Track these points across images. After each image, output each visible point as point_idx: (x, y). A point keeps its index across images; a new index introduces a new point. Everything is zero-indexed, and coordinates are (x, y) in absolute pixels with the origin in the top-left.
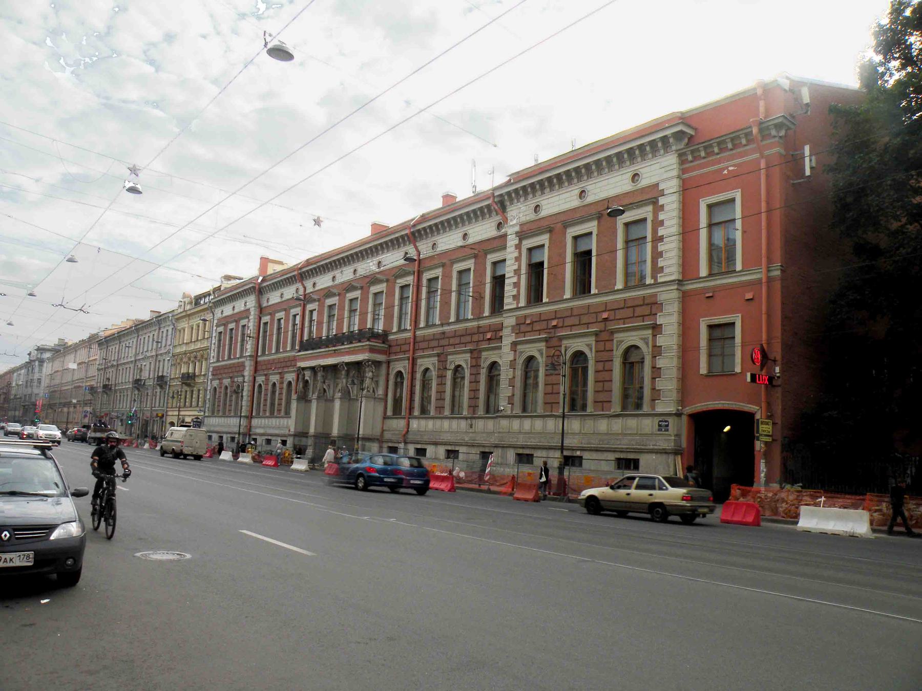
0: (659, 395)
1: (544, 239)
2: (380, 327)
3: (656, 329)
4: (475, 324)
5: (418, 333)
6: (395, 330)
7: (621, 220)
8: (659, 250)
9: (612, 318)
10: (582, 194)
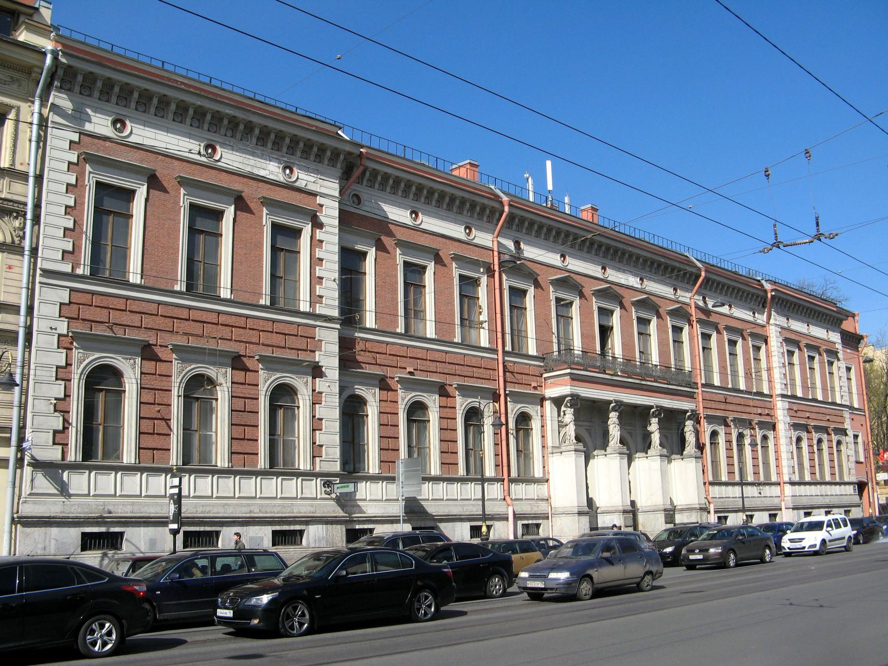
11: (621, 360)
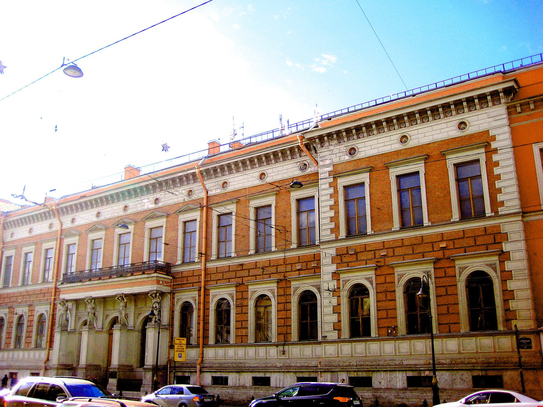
0: (515, 316)
1: (162, 222)
2: (161, 260)
3: (504, 256)
4: (281, 255)
5: (210, 265)
6: (179, 262)
7: (394, 172)
8: (497, 187)
9: (304, 268)
10: (98, 215)
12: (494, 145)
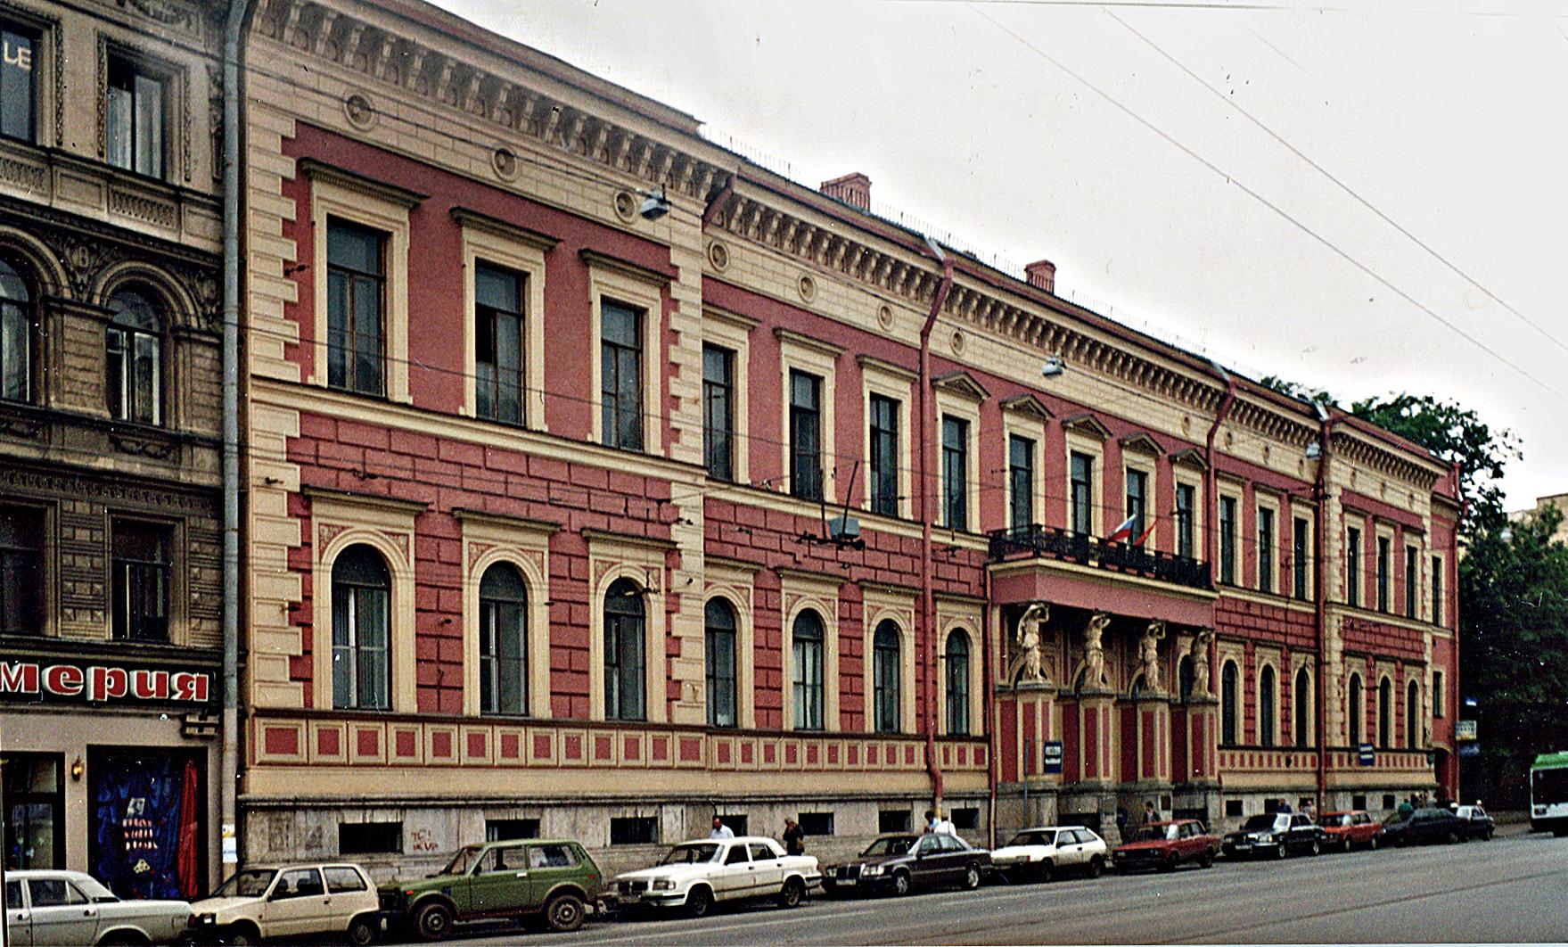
11: (1153, 554)
12: (676, 291)
